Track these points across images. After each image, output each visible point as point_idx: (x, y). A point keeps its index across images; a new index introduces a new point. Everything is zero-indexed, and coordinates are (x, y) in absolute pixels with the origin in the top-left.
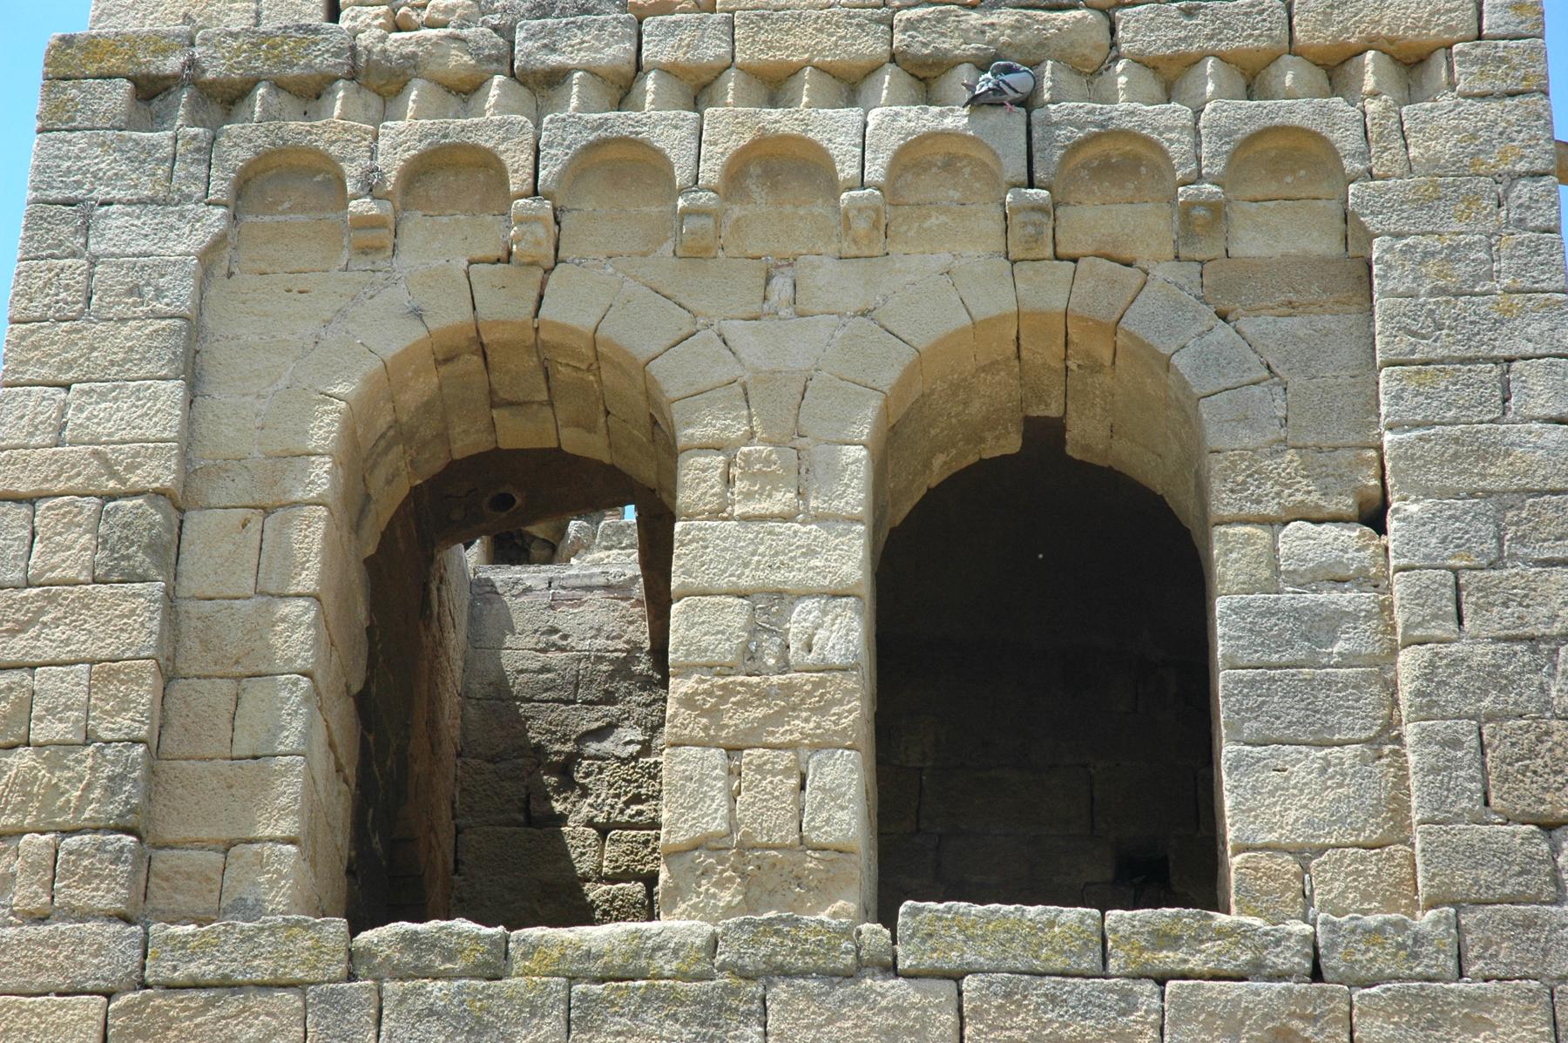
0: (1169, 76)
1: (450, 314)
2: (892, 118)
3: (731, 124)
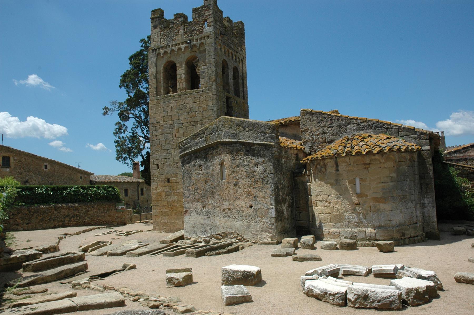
0: (197, 40)
1: (167, 61)
2: (185, 45)
3: (177, 47)
